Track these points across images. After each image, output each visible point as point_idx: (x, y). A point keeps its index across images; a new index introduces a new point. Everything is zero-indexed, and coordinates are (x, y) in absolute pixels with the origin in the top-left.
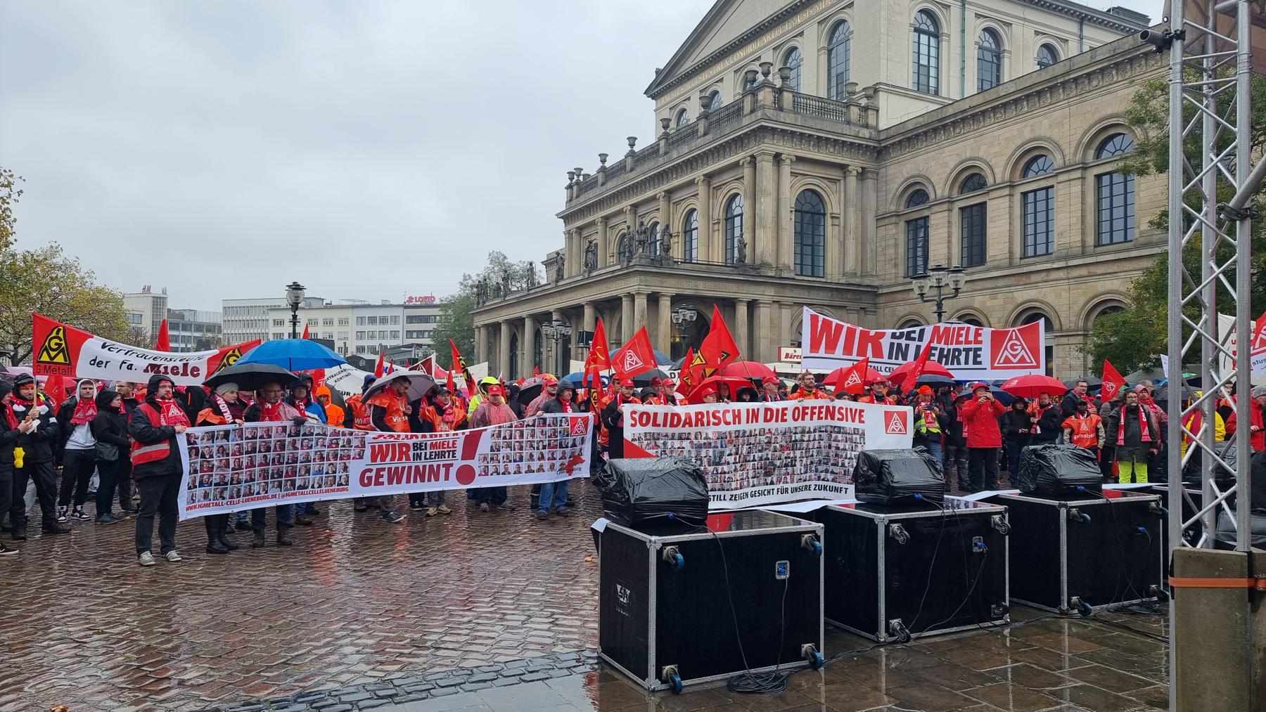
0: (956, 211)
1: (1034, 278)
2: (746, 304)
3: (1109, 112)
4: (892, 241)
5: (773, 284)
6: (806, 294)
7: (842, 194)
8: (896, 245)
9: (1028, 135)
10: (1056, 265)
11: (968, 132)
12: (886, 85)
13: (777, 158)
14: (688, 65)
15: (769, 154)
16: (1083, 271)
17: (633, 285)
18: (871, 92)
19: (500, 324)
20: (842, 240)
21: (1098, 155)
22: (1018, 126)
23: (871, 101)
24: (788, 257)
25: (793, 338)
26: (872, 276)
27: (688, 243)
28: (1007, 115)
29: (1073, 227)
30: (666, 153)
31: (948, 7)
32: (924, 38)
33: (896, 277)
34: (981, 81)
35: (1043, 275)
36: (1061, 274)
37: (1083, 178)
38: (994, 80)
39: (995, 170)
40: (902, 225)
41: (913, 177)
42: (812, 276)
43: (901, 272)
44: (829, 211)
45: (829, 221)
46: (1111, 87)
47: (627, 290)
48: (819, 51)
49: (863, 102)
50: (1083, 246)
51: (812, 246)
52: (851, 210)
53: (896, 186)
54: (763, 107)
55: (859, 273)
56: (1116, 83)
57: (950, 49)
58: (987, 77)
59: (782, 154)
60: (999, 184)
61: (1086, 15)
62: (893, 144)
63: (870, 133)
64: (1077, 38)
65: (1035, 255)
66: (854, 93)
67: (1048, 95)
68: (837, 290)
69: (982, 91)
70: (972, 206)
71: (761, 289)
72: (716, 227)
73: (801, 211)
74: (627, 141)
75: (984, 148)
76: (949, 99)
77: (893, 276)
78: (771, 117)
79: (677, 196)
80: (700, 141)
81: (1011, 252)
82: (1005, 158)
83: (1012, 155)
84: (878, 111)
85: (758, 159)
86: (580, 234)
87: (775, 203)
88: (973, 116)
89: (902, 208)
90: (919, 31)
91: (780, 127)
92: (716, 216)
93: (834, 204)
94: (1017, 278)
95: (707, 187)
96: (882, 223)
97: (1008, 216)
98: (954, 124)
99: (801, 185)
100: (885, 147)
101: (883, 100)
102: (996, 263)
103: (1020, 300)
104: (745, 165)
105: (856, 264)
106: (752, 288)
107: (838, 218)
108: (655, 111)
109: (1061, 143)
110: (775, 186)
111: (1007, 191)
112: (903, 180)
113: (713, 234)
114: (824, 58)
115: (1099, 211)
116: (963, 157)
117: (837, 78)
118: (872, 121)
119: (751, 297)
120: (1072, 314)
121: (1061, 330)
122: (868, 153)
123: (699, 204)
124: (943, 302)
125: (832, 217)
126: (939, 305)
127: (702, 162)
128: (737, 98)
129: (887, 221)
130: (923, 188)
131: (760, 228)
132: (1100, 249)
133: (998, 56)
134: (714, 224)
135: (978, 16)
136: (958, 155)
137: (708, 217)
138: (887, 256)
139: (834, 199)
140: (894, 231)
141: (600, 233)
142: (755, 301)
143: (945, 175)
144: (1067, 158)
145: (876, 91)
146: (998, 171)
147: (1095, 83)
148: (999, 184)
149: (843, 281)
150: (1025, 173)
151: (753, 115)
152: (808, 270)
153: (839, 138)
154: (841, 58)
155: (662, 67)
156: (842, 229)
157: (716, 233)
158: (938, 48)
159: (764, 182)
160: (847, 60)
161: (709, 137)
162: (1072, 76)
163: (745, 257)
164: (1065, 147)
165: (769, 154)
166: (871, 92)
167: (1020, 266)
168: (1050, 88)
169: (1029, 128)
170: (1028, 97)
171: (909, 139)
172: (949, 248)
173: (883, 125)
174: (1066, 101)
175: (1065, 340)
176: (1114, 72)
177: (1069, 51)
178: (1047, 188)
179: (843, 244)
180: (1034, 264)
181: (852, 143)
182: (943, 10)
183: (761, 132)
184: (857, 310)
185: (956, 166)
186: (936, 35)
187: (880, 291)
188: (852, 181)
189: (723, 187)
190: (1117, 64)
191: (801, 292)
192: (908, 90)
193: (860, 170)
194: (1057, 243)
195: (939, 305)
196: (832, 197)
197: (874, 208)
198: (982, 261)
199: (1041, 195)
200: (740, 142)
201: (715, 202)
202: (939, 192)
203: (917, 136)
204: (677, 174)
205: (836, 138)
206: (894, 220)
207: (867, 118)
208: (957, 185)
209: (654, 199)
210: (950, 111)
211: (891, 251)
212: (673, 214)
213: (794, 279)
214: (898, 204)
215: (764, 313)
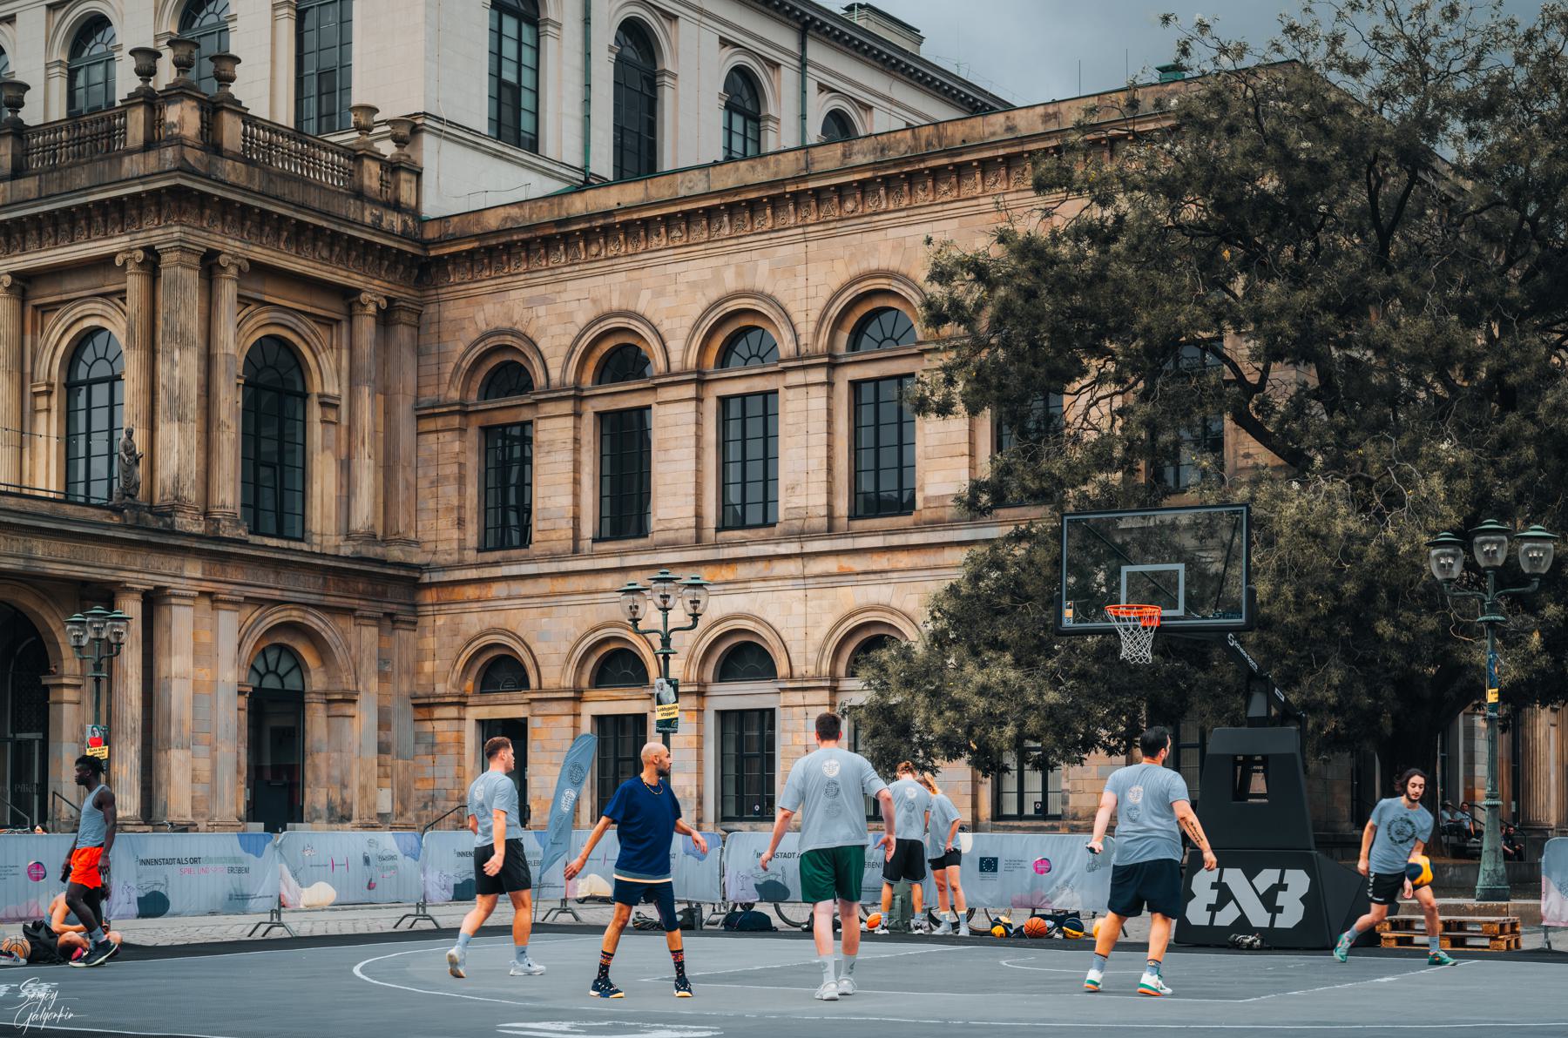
0: (588, 421)
2: (139, 596)
3: (874, 264)
4: (453, 469)
5: (199, 553)
6: (272, 576)
7: (345, 353)
8: (461, 480)
9: (731, 283)
10: (783, 549)
11: (616, 257)
12: (439, 119)
13: (209, 265)
16: (831, 565)
18: (404, 131)
20: (344, 456)
21: (854, 345)
22: (713, 262)
23: (407, 150)
26: (408, 542)
28: (693, 235)
29: (813, 477)
31: (775, 66)
35: (760, 566)
36: (792, 567)
37: (830, 384)
40: (473, 435)
41: (499, 332)
42: (279, 535)
44: (316, 387)
45: (315, 413)
46: (876, 218)
50: (831, 516)
53: (461, 348)
54: (179, 141)
55: (380, 533)
56: (886, 212)
59: (218, 253)
60: (678, 374)
61: (813, 19)
63: (405, 223)
64: (796, 63)
67: (769, 212)
68: (335, 572)
71: (171, 564)
72: (42, 402)
75: (646, 295)
77: (455, 545)
82: (689, 322)
84: (419, 175)
88: (626, 226)
91: (219, 193)
95: (18, 303)
97: (693, 442)
99: (259, 326)
100: (439, 258)
101: (430, 151)
102: (670, 535)
104: (131, 267)
105: (375, 517)
106: (156, 560)
107: (336, 406)
109: (791, 308)
110: (204, 326)
111: (690, 391)
112: (475, 336)
113: (33, 421)
114: (287, 28)
116: (606, 308)
118: (406, 194)
119: (149, 580)
120: (811, 648)
121: (791, 677)
122: (401, 268)
124: (672, 635)
125: (323, 405)
126: (666, 642)
129: (440, 423)
134: (36, 394)
135: (822, 88)
136: (594, 301)
138: (442, 501)
139: (328, 361)
140: (457, 446)
142: (160, 589)
143: (568, 341)
144: (802, 341)
145: (416, 130)
146: (676, 348)
147: (849, 205)
148: (678, 374)
149: (346, 550)
150: (723, 361)
152: (269, 522)
153: (342, 230)
157: (42, 418)
158: (537, 49)
162: (812, 185)
163: (137, 486)
164: (798, 318)
167: (716, 545)
168: (772, 199)
170: (731, 209)
172: (576, 495)
173: (430, 209)
174: (800, 230)
175: (797, 698)
176: (882, 192)
179: (346, 467)
180: (742, 544)
181: (368, 243)
184: (377, 619)
187: (426, 578)
188: (366, 327)
189: (63, 309)
190: (886, 179)
192: (478, 133)
193: (383, 304)
195: (666, 642)
196: (323, 357)
201: (40, 342)
202: (555, 374)
203: (508, 247)
207: (397, 187)
208: (592, 365)
211: (450, 491)
213: (244, 543)
214: (466, 388)
215: (181, 621)
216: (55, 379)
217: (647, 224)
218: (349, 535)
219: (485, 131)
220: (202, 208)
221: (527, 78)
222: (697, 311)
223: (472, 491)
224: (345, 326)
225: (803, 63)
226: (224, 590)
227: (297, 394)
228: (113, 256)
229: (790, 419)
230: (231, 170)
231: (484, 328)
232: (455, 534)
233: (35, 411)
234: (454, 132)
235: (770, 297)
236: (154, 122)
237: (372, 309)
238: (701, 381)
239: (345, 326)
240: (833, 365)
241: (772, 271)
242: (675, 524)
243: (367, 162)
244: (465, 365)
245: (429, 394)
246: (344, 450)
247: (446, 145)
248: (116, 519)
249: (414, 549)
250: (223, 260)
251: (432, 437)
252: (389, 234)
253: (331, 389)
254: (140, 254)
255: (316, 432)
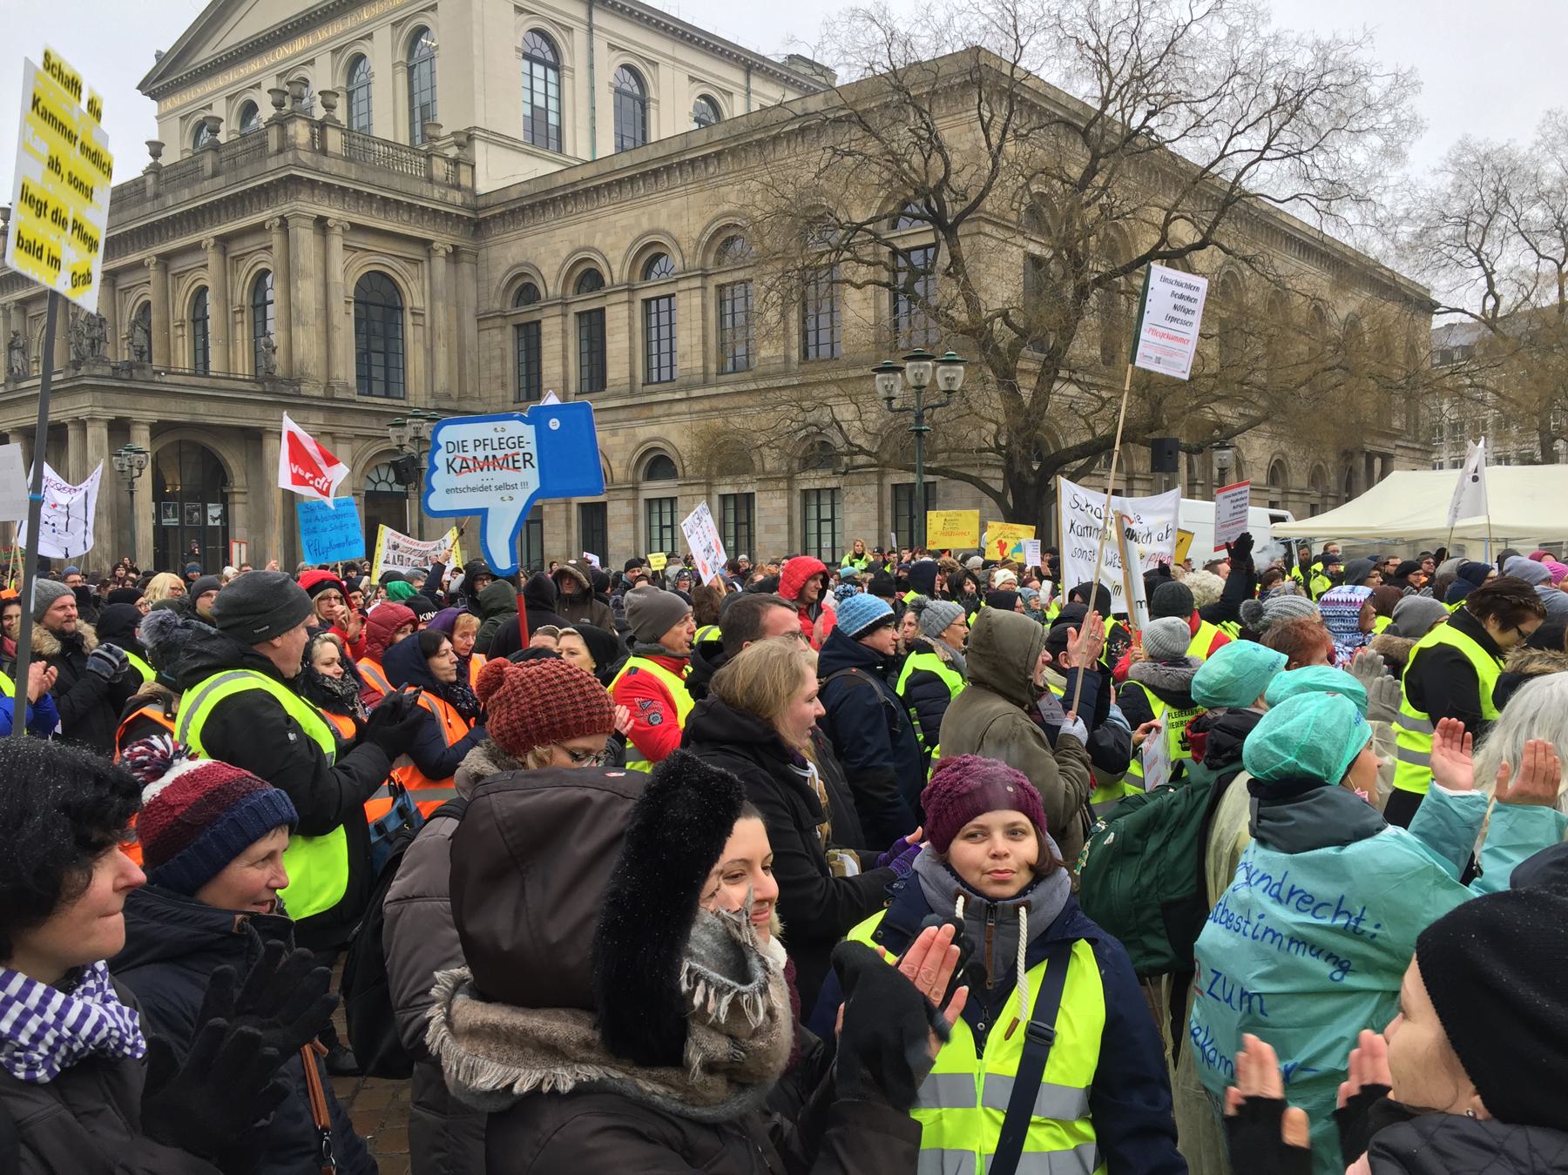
0: (571, 317)
1: (658, 410)
4: (497, 352)
5: (320, 408)
6: (375, 421)
8: (503, 359)
9: (646, 225)
10: (677, 396)
12: (485, 131)
13: (321, 223)
14: (206, 54)
15: (308, 218)
17: (82, 406)
18: (463, 139)
19: (65, 425)
20: (428, 346)
21: (719, 263)
22: (635, 212)
23: (465, 151)
24: (346, 370)
25: (356, 486)
26: (473, 399)
27: (260, 325)
28: (778, 154)
29: (694, 349)
30: (157, 196)
31: (569, 30)
32: (539, 70)
33: (504, 402)
34: (620, 136)
36: (683, 407)
37: (703, 288)
38: (639, 137)
39: (613, 267)
40: (510, 329)
41: (518, 265)
42: (387, 396)
43: (511, 396)
44: (408, 303)
45: (409, 319)
47: (75, 413)
48: (394, 66)
49: (452, 152)
50: (706, 373)
51: (386, 353)
52: (440, 305)
53: (500, 275)
57: (576, 87)
58: (628, 132)
62: (494, 217)
63: (464, 198)
65: (659, 381)
66: (438, 139)
69: (621, 149)
70: (590, 312)
72: (239, 317)
73: (366, 303)
74: (147, 149)
75: (599, 236)
76: (576, 159)
78: (309, 163)
79: (178, 265)
80: (207, 185)
81: (632, 376)
82: (623, 252)
83: (630, 249)
84: (473, 167)
85: (291, 223)
86: (25, 312)
87: (321, 290)
88: (586, 191)
89: (509, 306)
90: (530, 58)
91: (322, 179)
92: (238, 301)
93: (414, 295)
94: (639, 409)
95: (221, 257)
96: (485, 325)
97: (627, 329)
98: (564, 198)
99: (362, 265)
100: (485, 218)
103: (641, 438)
108: (157, 118)
110: (320, 264)
111: (625, 296)
114: (402, 78)
115: (648, 344)
116: (577, 246)
117: (422, 113)
118: (465, 180)
123: (209, 278)
125: (413, 314)
127: (211, 218)
128: (187, 155)
129: (490, 323)
130: (593, 266)
131: (297, 325)
132: (723, 378)
133: (643, 103)
135: (612, 47)
137: (226, 301)
140: (499, 338)
141: (276, 250)
143: (557, 268)
145: (470, 138)
146: (616, 268)
149: (430, 406)
150: (647, 272)
151: (281, 156)
152: (378, 387)
154: (426, 83)
155: (165, 50)
156: (428, 331)
157: (239, 327)
158: (559, 85)
159: (301, 257)
160: (433, 87)
161: (220, 180)
162: (688, 157)
163: (274, 367)
165: (308, 218)
166: (463, 139)
169: (646, 216)
170: (644, 175)
171: (512, 212)
172: (565, 366)
173: (483, 186)
177: (735, 108)
178: (670, 296)
179: (430, 352)
180: (654, 393)
182: (563, 33)
183: (290, 185)
185: (569, 257)
186: (556, 67)
188: (440, 265)
189: (246, 257)
191: (366, 419)
192: (515, 140)
193: (450, 249)
194: (682, 365)
196: (411, 285)
197: (473, 303)
198: (603, 386)
199: (740, 292)
200: (265, 194)
201: (236, 278)
203: (522, 209)
204: (174, 230)
205: (410, 201)
206: (499, 322)
209: (139, 265)
210: (577, 175)
211: (496, 366)
212: (174, 292)
213: (354, 401)
216: (245, 303)
217: (597, 189)
218: (433, 395)
219: (521, 139)
220: (313, 189)
221: (553, 105)
222: (627, 244)
223: (510, 365)
224: (426, 264)
225: (590, 28)
226: (340, 431)
227: (397, 308)
228: (263, 223)
229: (681, 312)
230: (327, 164)
231: (511, 261)
232: (500, 393)
233: (235, 323)
234: (499, 140)
235: (668, 233)
236: (283, 136)
237: (442, 253)
238: (631, 290)
239: (426, 264)
240: (705, 275)
241: (669, 216)
242: (619, 382)
243: (434, 159)
244: (503, 286)
245: (484, 307)
246: (428, 343)
247: (492, 148)
248: (259, 389)
249: (477, 402)
250: (330, 223)
251: (486, 332)
252: (453, 205)
253: (418, 304)
254: (278, 220)
255: (410, 331)
